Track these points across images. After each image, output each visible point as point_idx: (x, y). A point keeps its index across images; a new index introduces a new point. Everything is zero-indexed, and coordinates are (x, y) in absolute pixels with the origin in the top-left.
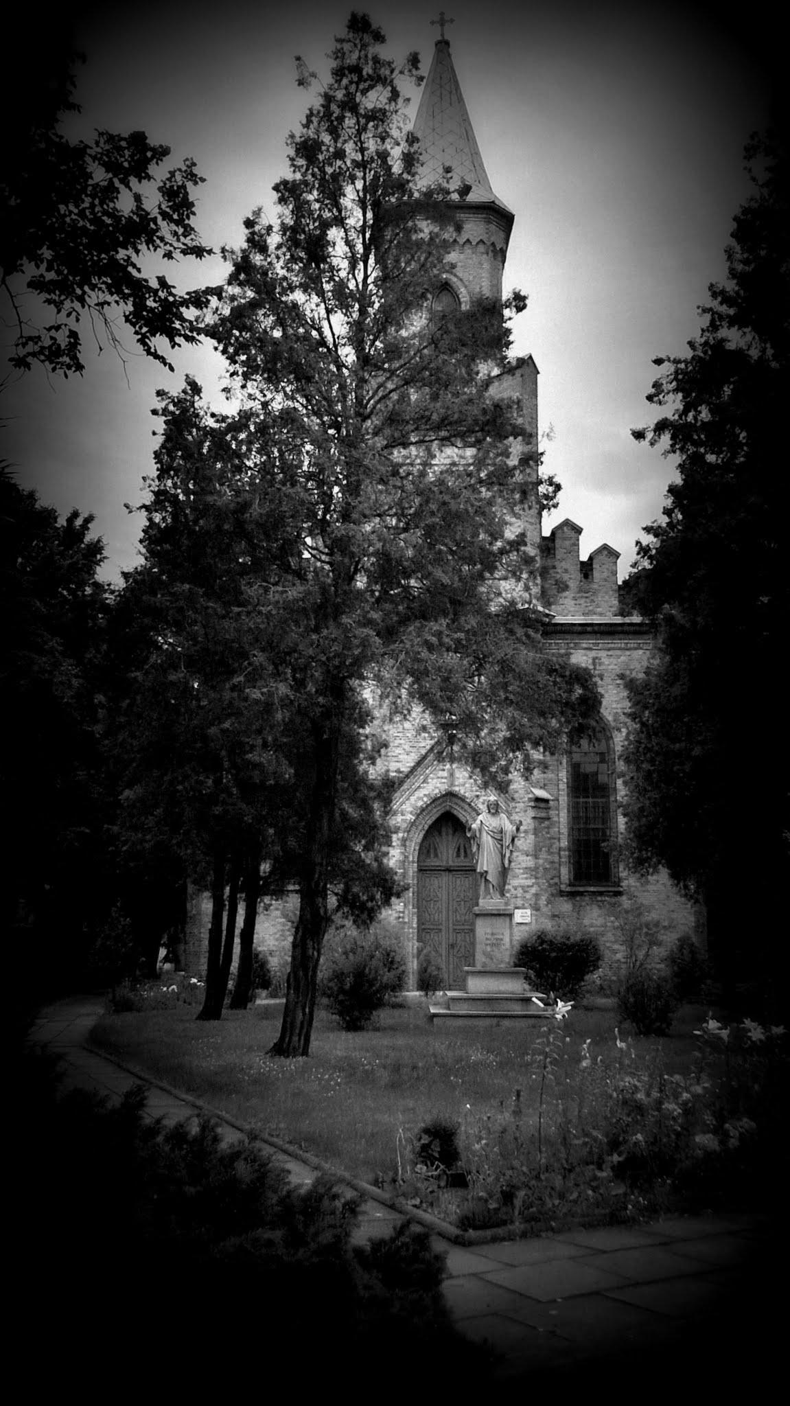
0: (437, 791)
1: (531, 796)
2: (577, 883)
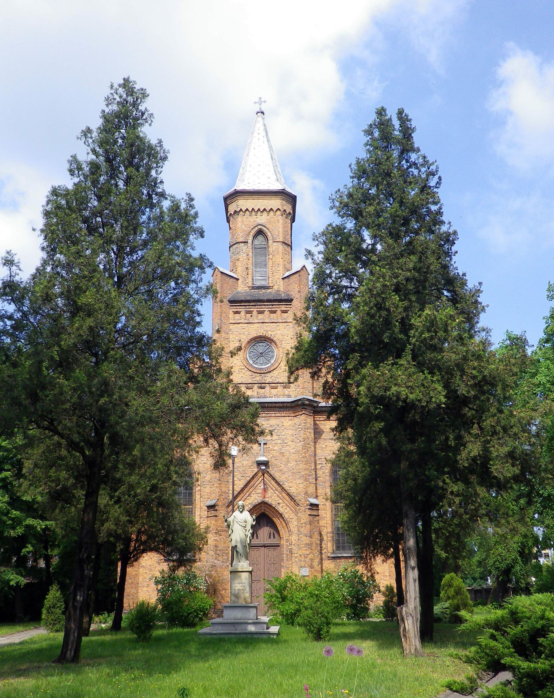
0: (256, 501)
1: (307, 503)
2: (337, 552)
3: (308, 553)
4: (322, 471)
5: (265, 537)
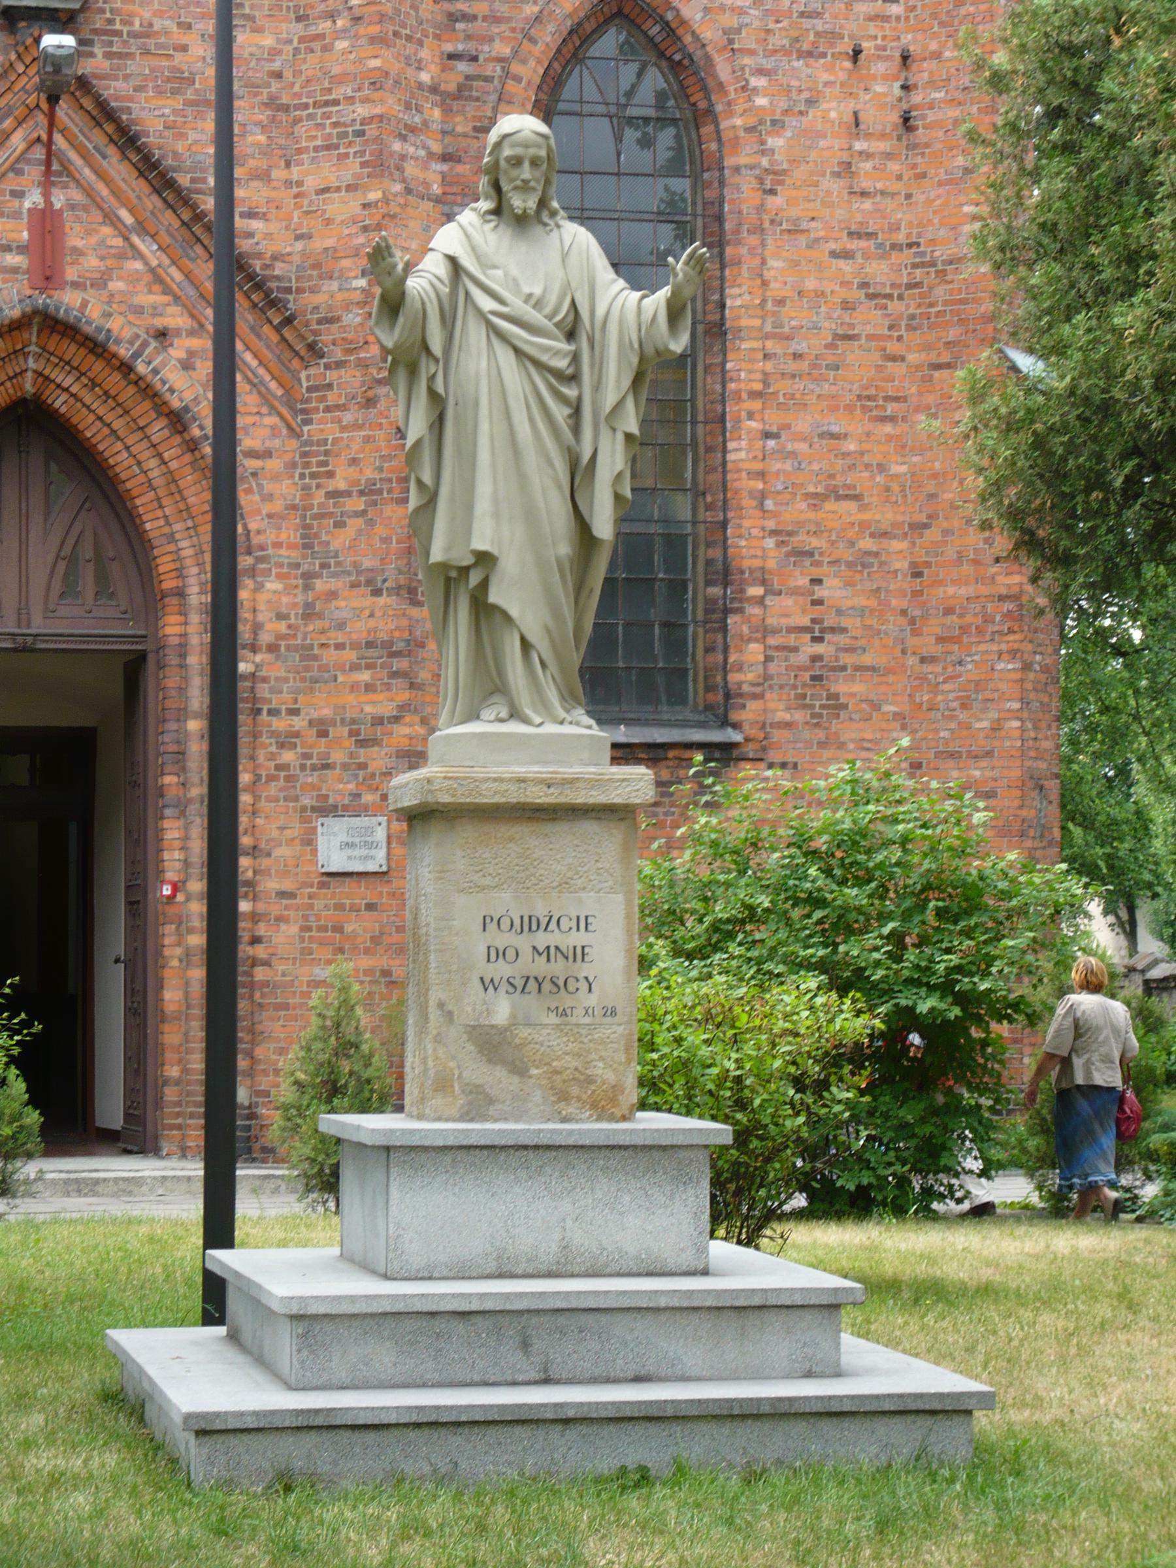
3: (387, 708)
4: (471, 109)
5: (38, 579)
